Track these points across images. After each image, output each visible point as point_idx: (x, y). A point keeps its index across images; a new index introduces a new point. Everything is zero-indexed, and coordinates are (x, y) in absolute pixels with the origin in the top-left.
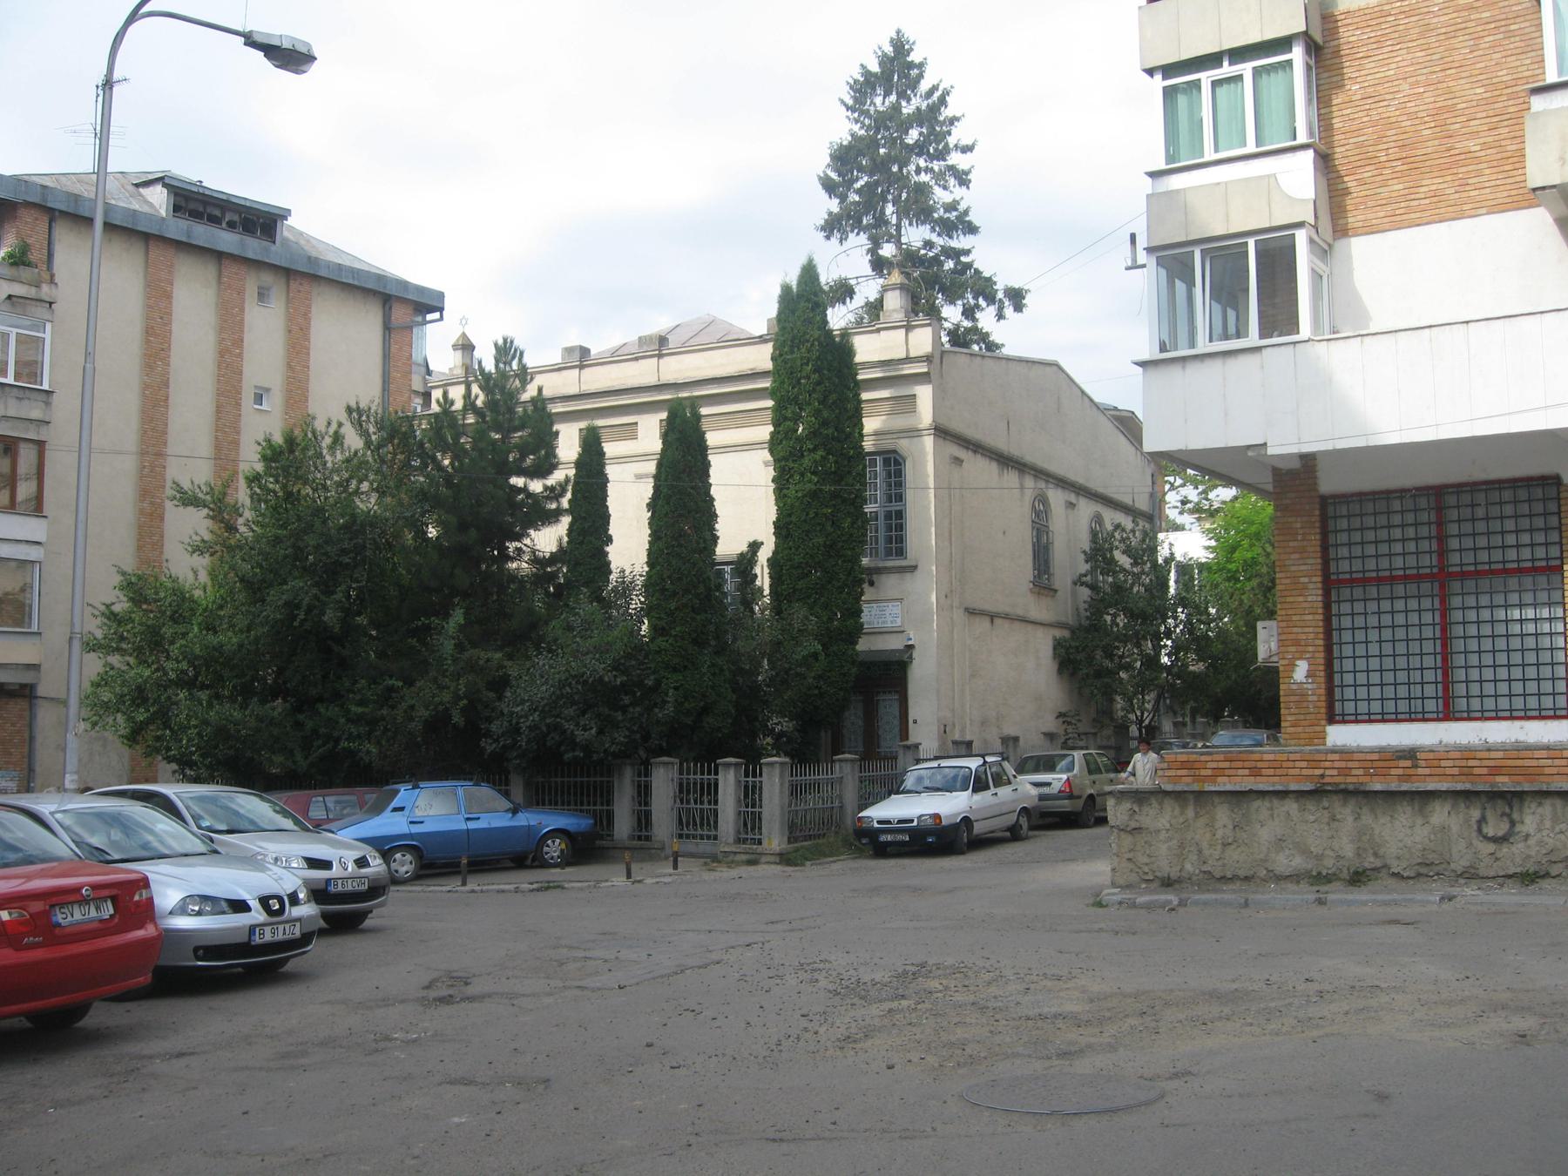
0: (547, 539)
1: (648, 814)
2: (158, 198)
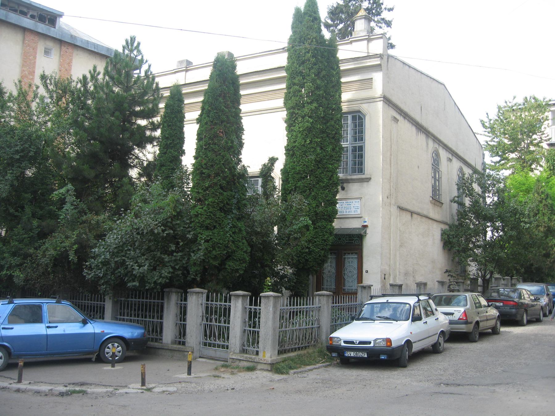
0: (149, 153)
1: (184, 326)
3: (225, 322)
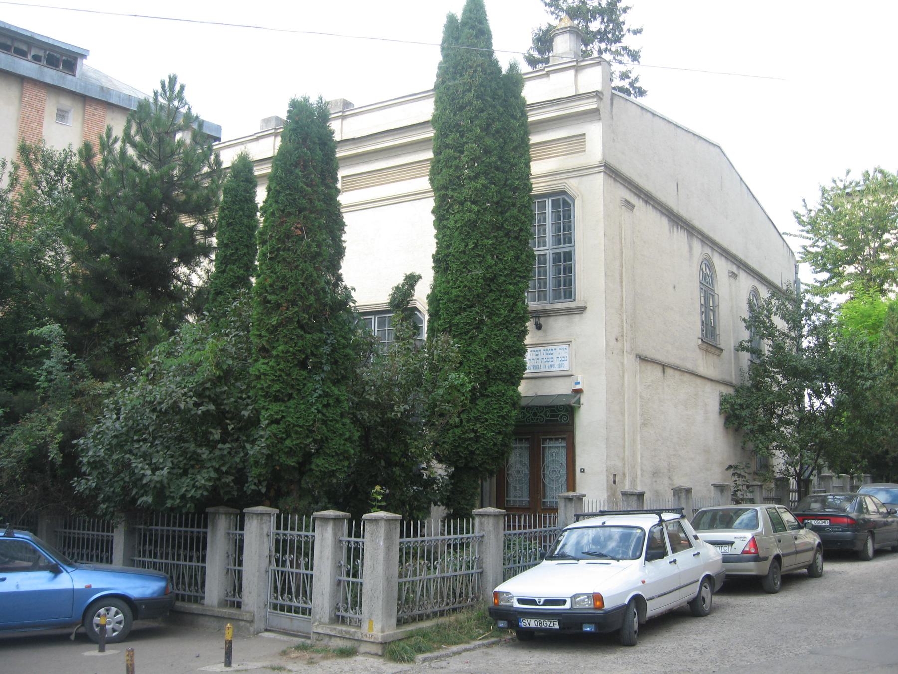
3: (307, 569)
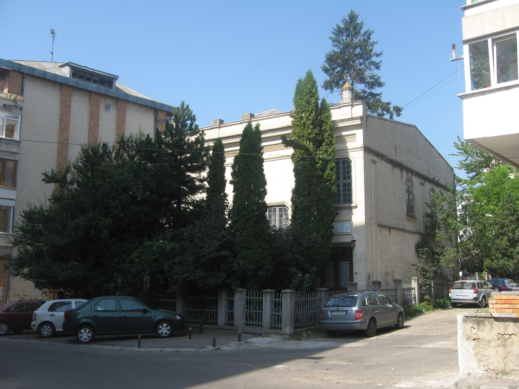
1: (232, 314)
2: (66, 72)
3: (259, 310)
